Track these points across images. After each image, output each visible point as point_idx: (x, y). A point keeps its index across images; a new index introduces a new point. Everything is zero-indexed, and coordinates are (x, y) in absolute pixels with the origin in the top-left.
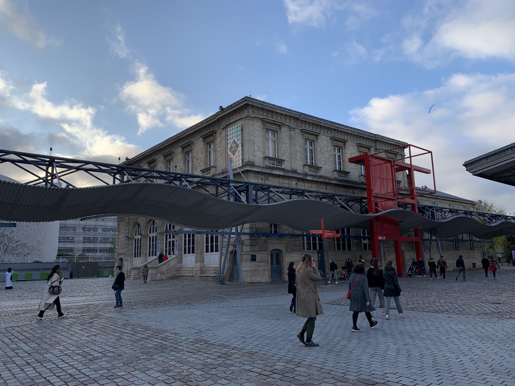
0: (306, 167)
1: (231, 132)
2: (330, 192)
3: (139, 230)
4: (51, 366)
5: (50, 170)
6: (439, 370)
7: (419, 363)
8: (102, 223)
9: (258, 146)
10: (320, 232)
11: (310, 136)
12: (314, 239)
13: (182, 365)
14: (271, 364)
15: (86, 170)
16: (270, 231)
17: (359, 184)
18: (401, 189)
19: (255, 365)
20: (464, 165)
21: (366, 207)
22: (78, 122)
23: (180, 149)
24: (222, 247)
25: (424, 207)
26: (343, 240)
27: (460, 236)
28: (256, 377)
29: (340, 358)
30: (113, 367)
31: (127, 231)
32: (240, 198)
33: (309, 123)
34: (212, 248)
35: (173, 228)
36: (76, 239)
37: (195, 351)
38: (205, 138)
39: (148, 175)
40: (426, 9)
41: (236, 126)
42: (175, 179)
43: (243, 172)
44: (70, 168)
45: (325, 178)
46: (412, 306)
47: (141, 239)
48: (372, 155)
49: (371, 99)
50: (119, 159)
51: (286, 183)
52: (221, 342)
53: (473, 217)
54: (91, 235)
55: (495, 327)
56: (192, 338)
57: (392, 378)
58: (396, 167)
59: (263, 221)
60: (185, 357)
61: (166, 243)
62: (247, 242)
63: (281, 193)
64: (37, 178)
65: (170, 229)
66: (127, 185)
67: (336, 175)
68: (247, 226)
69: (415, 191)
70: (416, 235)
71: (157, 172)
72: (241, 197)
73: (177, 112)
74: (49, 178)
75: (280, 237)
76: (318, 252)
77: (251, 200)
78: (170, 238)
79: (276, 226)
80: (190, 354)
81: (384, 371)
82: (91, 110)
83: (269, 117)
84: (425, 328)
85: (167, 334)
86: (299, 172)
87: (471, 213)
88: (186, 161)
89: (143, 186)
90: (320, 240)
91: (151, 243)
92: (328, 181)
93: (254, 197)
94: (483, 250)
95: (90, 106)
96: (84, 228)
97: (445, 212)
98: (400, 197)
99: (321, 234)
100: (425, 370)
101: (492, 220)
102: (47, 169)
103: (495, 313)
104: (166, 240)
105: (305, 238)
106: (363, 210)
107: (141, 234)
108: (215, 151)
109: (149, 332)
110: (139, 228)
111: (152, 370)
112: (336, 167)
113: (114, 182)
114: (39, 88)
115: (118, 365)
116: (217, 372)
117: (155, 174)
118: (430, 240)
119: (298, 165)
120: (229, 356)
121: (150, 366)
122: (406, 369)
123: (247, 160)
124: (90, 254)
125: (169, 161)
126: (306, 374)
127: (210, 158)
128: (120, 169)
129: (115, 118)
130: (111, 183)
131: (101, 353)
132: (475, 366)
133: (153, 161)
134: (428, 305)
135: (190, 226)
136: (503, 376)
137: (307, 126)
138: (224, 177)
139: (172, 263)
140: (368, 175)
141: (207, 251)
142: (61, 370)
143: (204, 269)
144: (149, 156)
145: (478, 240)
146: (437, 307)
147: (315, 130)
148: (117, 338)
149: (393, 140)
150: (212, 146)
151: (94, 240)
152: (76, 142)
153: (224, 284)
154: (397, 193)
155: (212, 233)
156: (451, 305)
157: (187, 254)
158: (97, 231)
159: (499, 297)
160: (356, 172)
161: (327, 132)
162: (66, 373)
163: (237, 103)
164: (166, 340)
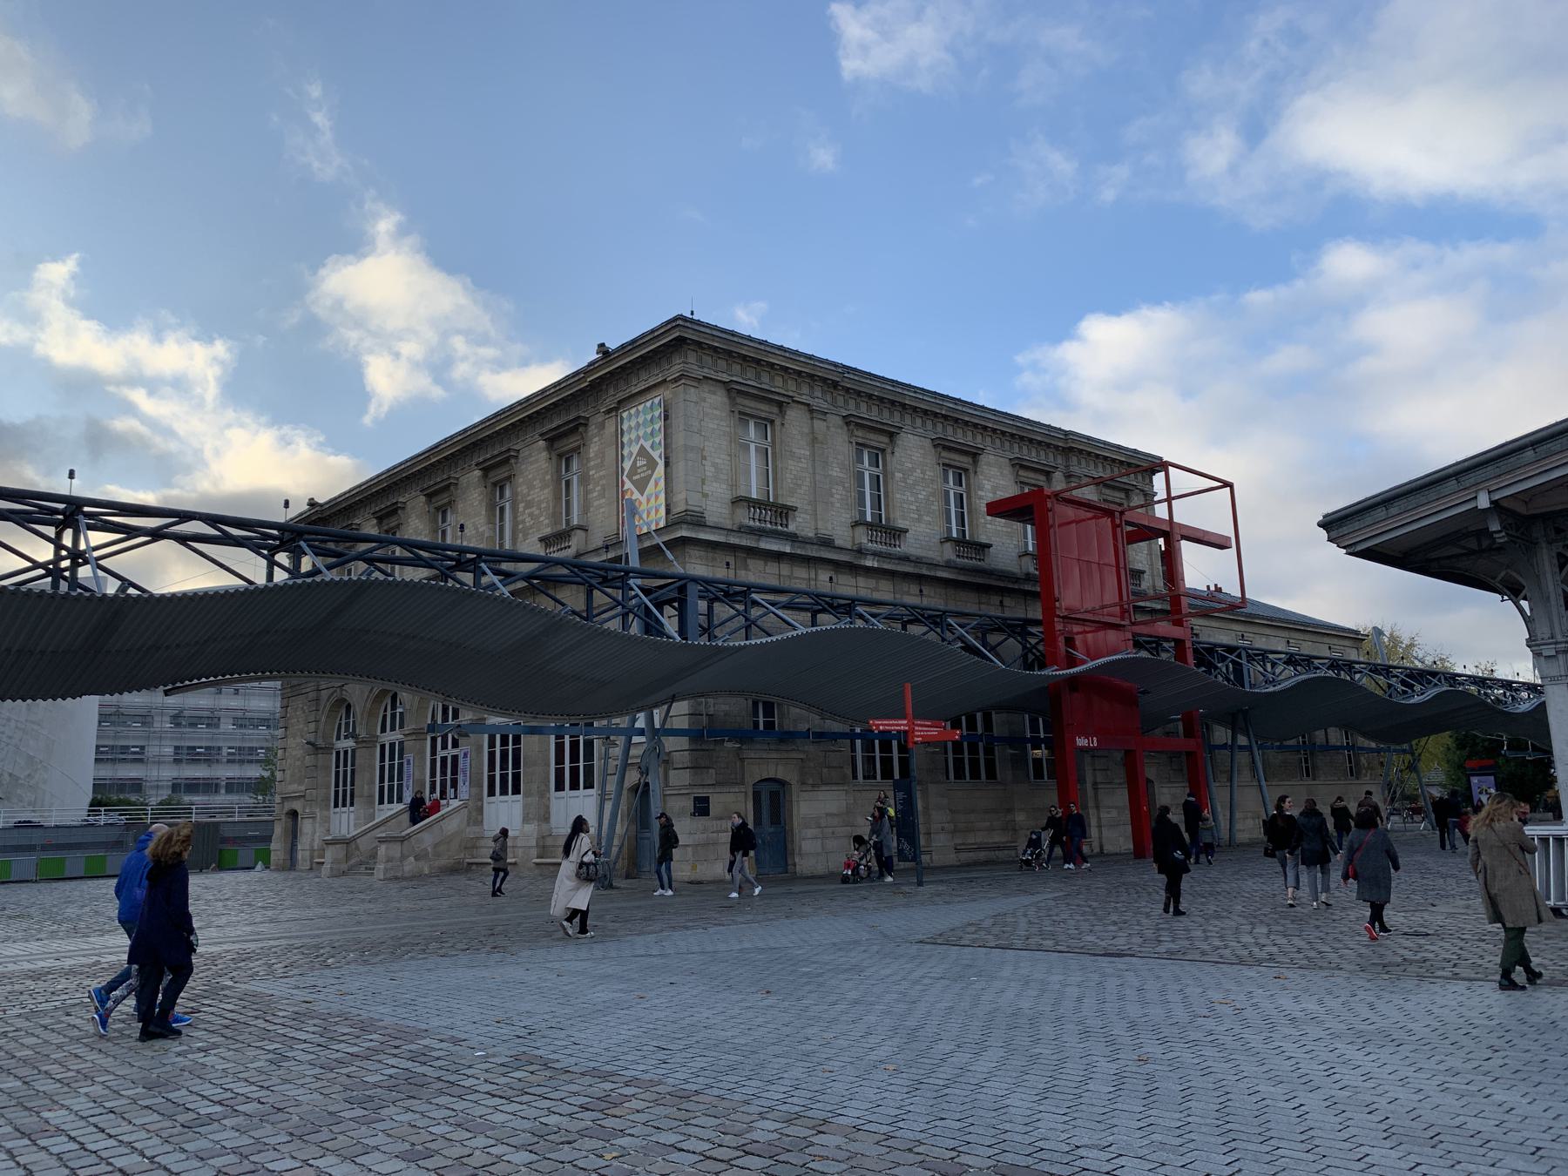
0: (861, 530)
1: (633, 424)
2: (932, 606)
3: (347, 724)
4: (60, 1145)
5: (67, 540)
6: (1232, 1135)
7: (1177, 1115)
8: (235, 702)
9: (714, 465)
10: (901, 725)
11: (872, 436)
12: (886, 747)
13: (470, 1135)
14: (739, 1127)
15: (183, 539)
16: (757, 720)
17: (1016, 580)
18: (1142, 596)
19: (692, 1130)
20: (1319, 525)
21: (1041, 647)
22: (179, 385)
23: (477, 473)
24: (605, 774)
25: (1212, 649)
26: (973, 749)
27: (1319, 736)
28: (692, 1166)
29: (945, 1106)
30: (259, 1147)
31: (312, 726)
32: (662, 625)
33: (870, 396)
34: (574, 778)
35: (456, 716)
36: (152, 751)
37: (510, 1093)
38: (552, 440)
39: (379, 553)
40: (1253, 45)
41: (648, 404)
42: (461, 565)
43: (674, 544)
44: (131, 532)
45: (918, 561)
46: (1172, 946)
47: (353, 751)
48: (1056, 495)
49: (1080, 318)
50: (287, 504)
51: (799, 578)
52: (592, 1064)
53: (1357, 676)
54: (200, 738)
55: (1409, 1006)
56: (504, 1053)
57: (1096, 1160)
58: (1130, 528)
59: (731, 692)
60: (479, 1111)
61: (433, 762)
62: (682, 758)
63: (787, 607)
64: (29, 564)
65: (445, 719)
66: (309, 585)
67: (949, 553)
68: (681, 708)
69: (1185, 601)
70: (1189, 732)
71: (404, 544)
72: (664, 620)
73: (489, 352)
74: (65, 564)
75: (782, 741)
76: (897, 787)
77: (692, 629)
78: (444, 747)
79: (769, 709)
80: (497, 1101)
81: (1074, 1141)
82: (220, 348)
83: (749, 378)
84: (1205, 1012)
85: (426, 1042)
86: (838, 542)
87: (1349, 666)
88: (495, 511)
89: (360, 588)
90: (903, 749)
91: (387, 763)
92: (925, 572)
93: (703, 620)
94: (1387, 775)
95: (221, 336)
96: (177, 719)
97: (1274, 665)
98: (1140, 618)
99: (905, 732)
100: (1192, 1136)
101: (1411, 687)
102: (59, 535)
103: (1411, 962)
104: (434, 753)
105: (858, 742)
106: (1031, 657)
107: (354, 736)
108: (585, 480)
109: (374, 1036)
110: (348, 717)
111: (377, 1154)
112: (949, 530)
113: (270, 576)
114: (58, 272)
115: (272, 1141)
116: (576, 1154)
117: (399, 551)
118: (1232, 747)
119: (837, 523)
120: (616, 1105)
121: (371, 1142)
122: (1139, 1134)
123: (682, 508)
124: (196, 798)
125: (443, 511)
126: (843, 1155)
127: (568, 502)
128: (287, 536)
129: (295, 373)
130: (260, 579)
131: (220, 1103)
132: (1338, 1119)
133: (394, 511)
134: (1217, 943)
135: (504, 710)
136: (1416, 1149)
137: (863, 407)
138: (611, 561)
139: (452, 825)
140: (1043, 554)
141: (560, 787)
142: (93, 1159)
143: (549, 842)
144: (380, 496)
145: (1373, 745)
146: (1245, 946)
147: (886, 417)
148: (270, 1056)
149: (1119, 447)
150: (575, 465)
151: (209, 756)
152: (173, 446)
153: (611, 886)
154: (1131, 606)
155: (575, 731)
156: (1284, 941)
157: (498, 797)
158: (217, 726)
159: (1426, 916)
160: (1009, 544)
161: (924, 424)
162: (110, 1168)
163: (652, 335)
164: (422, 1059)
